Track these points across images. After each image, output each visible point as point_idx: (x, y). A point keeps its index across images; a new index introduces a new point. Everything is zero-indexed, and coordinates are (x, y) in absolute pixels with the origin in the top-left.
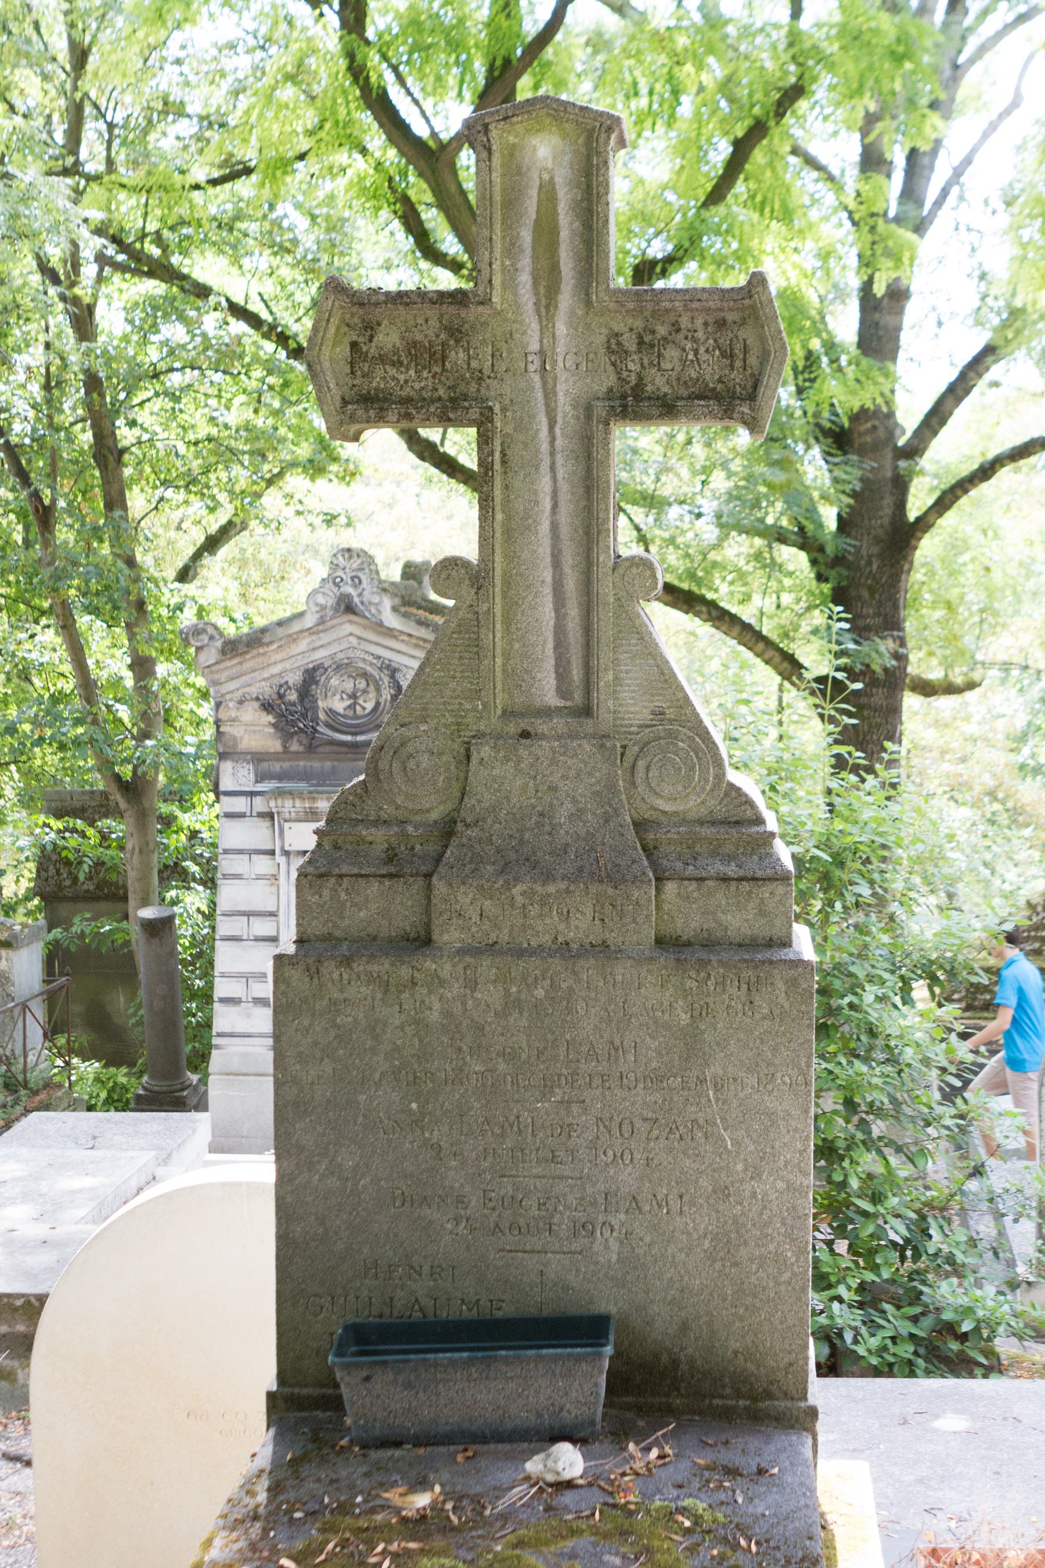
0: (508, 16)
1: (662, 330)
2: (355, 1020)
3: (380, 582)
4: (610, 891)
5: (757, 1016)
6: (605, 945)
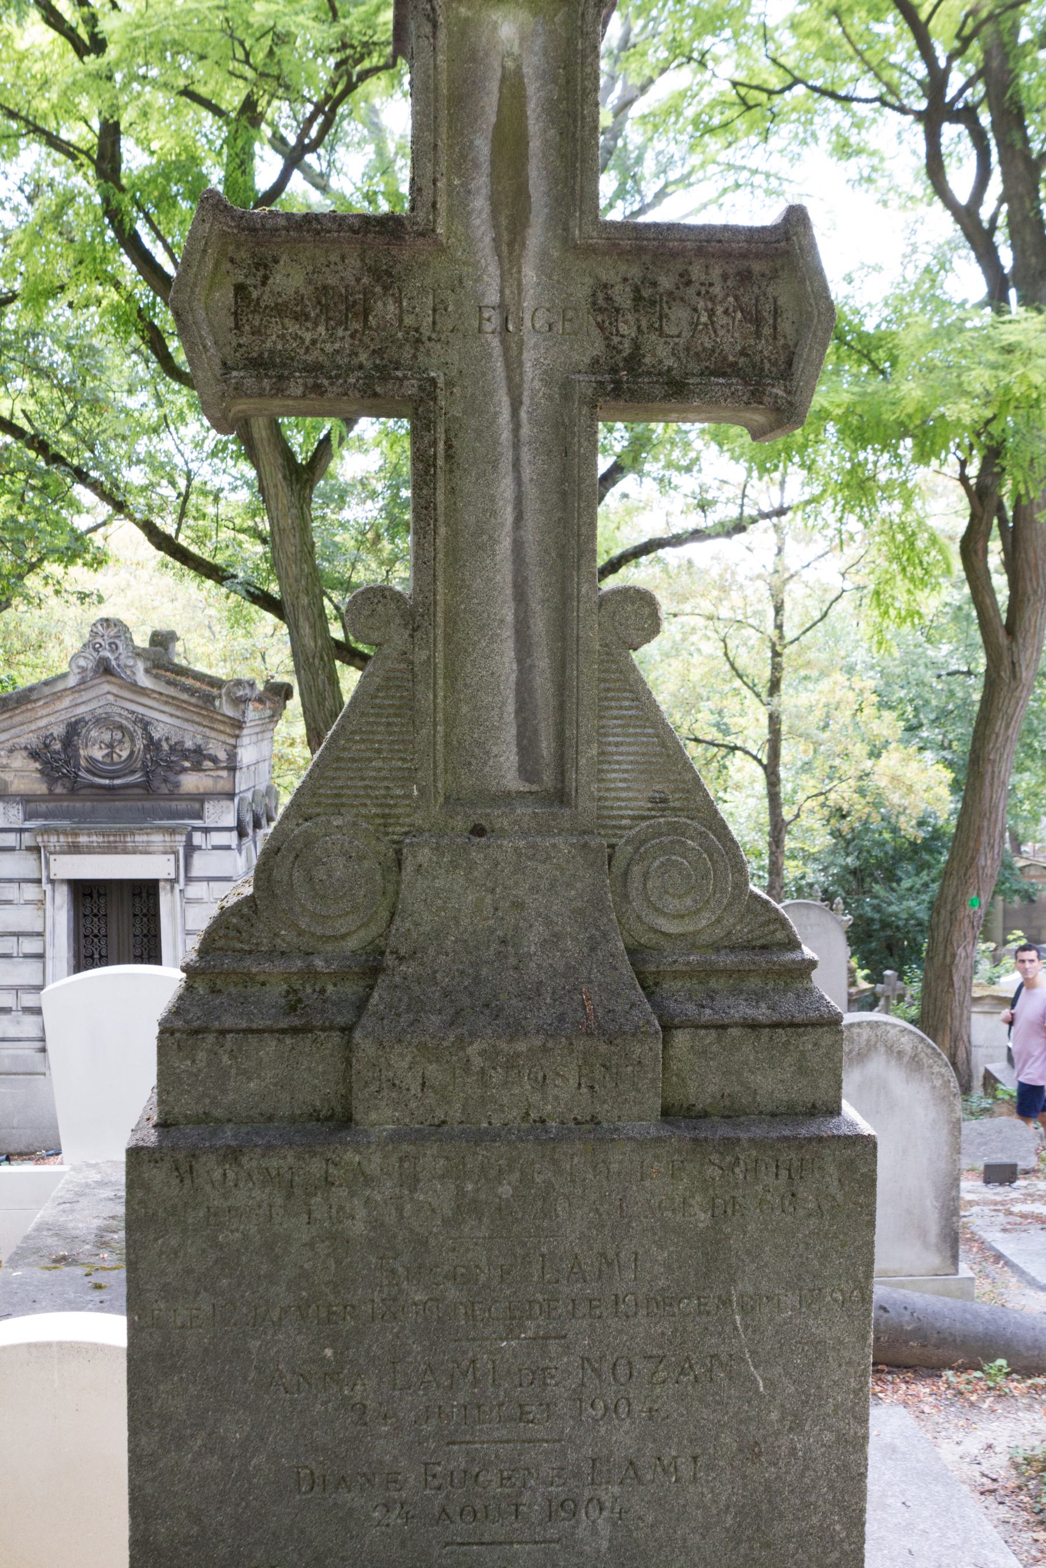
0: (244, 172)
1: (666, 282)
2: (245, 1236)
3: (134, 647)
4: (603, 1048)
5: (801, 1212)
6: (594, 1120)
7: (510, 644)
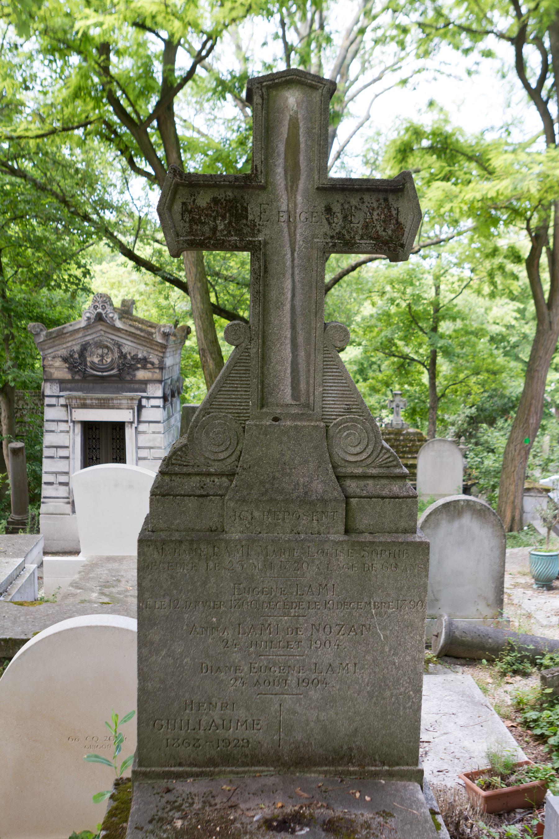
7: (289, 346)
